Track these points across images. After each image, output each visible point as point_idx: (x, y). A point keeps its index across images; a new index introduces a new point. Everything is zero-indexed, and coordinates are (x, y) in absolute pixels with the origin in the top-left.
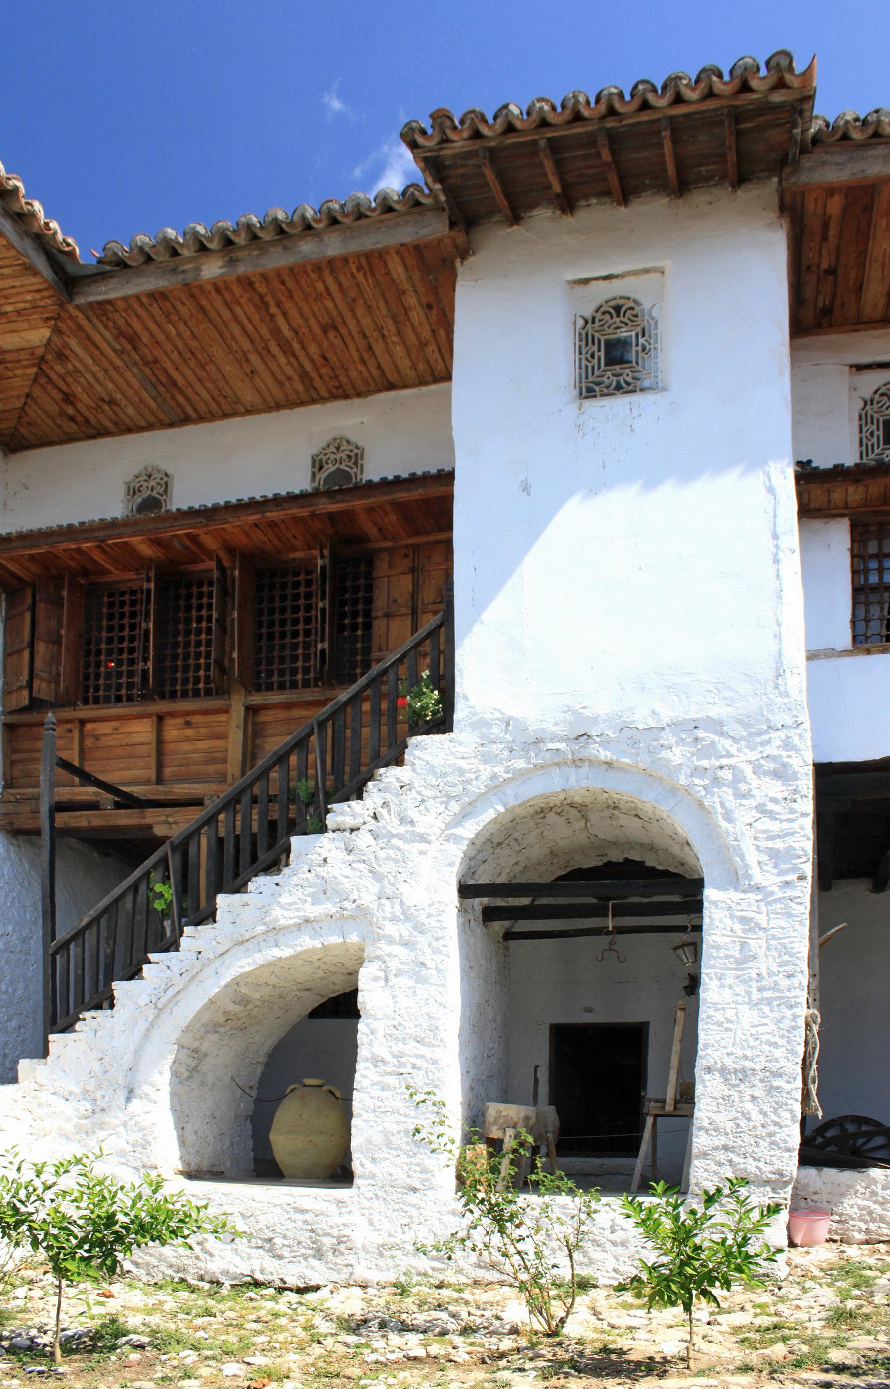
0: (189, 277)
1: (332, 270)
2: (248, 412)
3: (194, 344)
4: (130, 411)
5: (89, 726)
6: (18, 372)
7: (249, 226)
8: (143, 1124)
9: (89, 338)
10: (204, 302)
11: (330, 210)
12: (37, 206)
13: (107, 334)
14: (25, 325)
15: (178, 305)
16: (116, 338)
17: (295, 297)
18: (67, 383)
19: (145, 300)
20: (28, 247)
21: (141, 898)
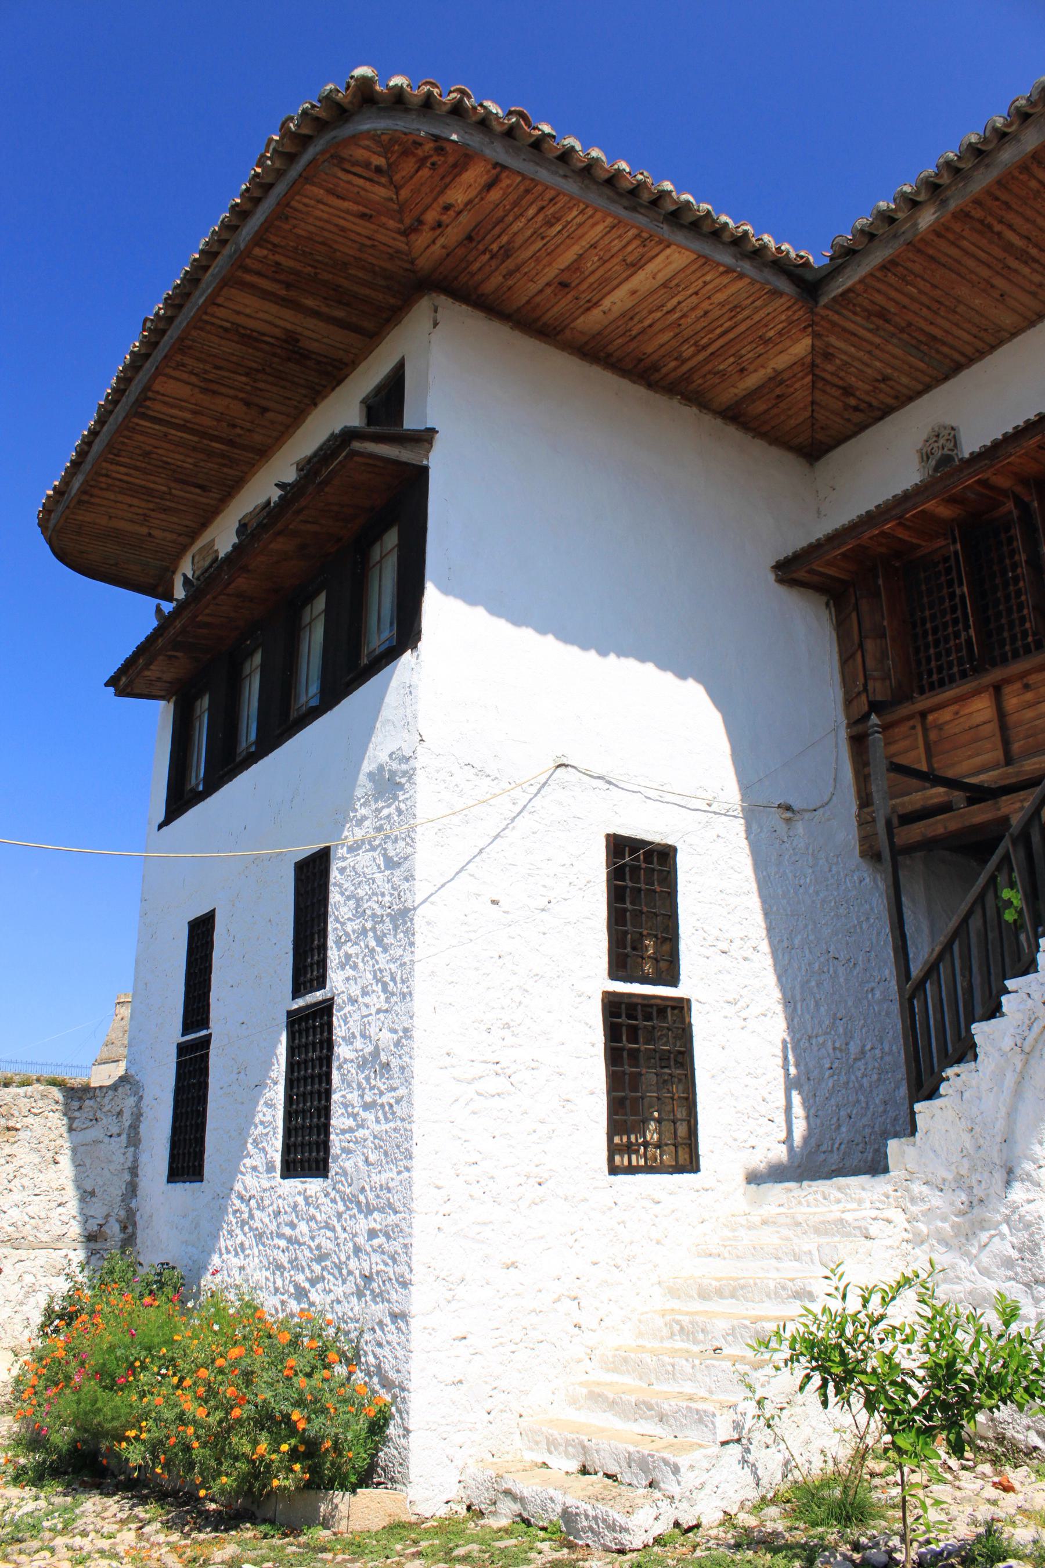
0: (909, 236)
1: (1039, 163)
2: (1014, 335)
3: (937, 293)
4: (904, 380)
5: (930, 718)
6: (797, 385)
7: (948, 164)
8: (1028, 1218)
9: (844, 330)
10: (931, 252)
11: (1017, 109)
12: (766, 238)
13: (858, 319)
14: (788, 343)
15: (909, 265)
16: (868, 319)
17: (1014, 206)
18: (841, 379)
19: (878, 274)
20: (768, 275)
21: (991, 912)
